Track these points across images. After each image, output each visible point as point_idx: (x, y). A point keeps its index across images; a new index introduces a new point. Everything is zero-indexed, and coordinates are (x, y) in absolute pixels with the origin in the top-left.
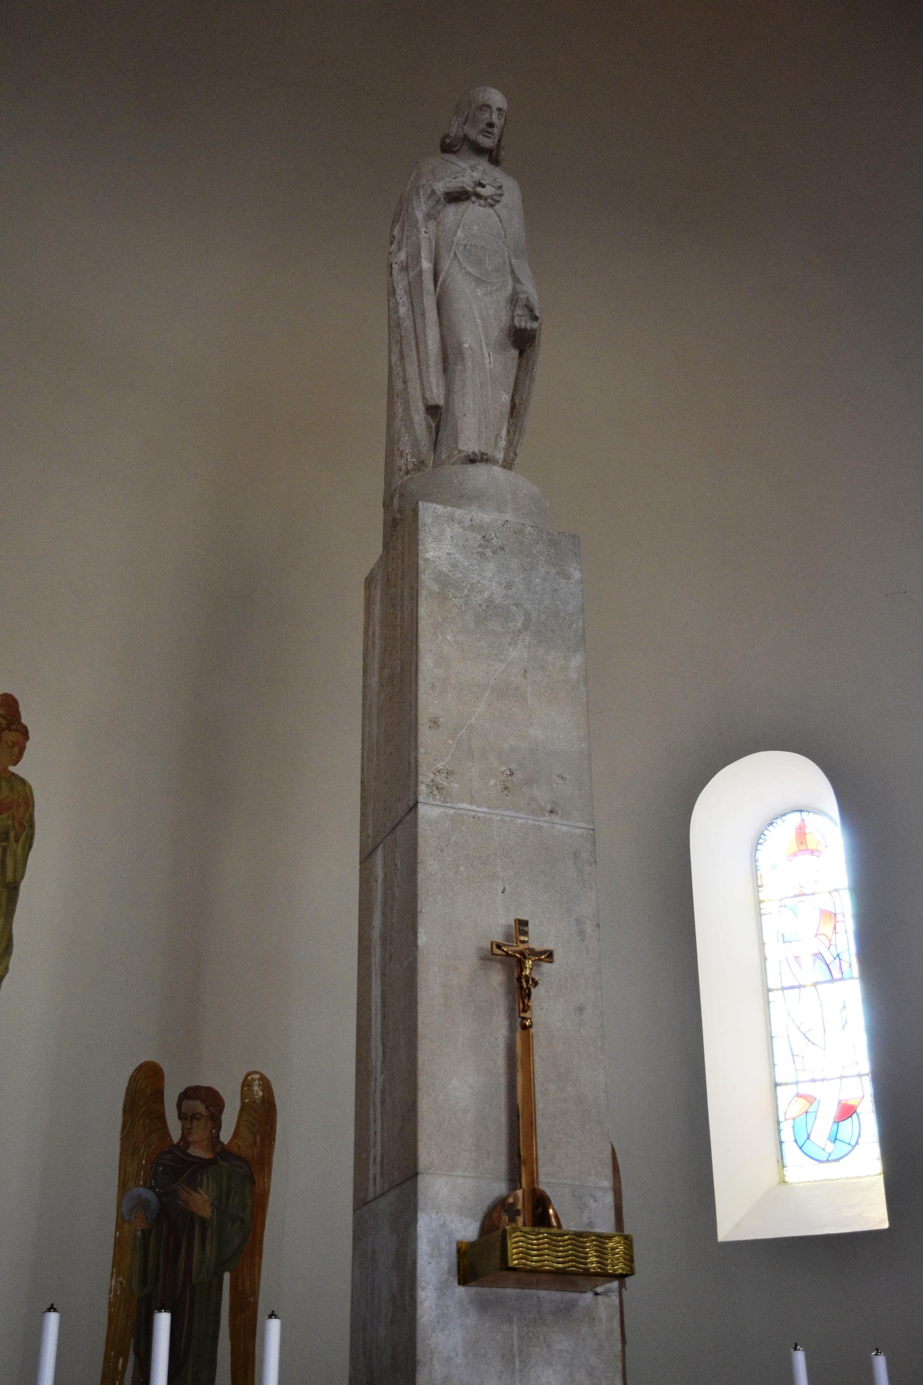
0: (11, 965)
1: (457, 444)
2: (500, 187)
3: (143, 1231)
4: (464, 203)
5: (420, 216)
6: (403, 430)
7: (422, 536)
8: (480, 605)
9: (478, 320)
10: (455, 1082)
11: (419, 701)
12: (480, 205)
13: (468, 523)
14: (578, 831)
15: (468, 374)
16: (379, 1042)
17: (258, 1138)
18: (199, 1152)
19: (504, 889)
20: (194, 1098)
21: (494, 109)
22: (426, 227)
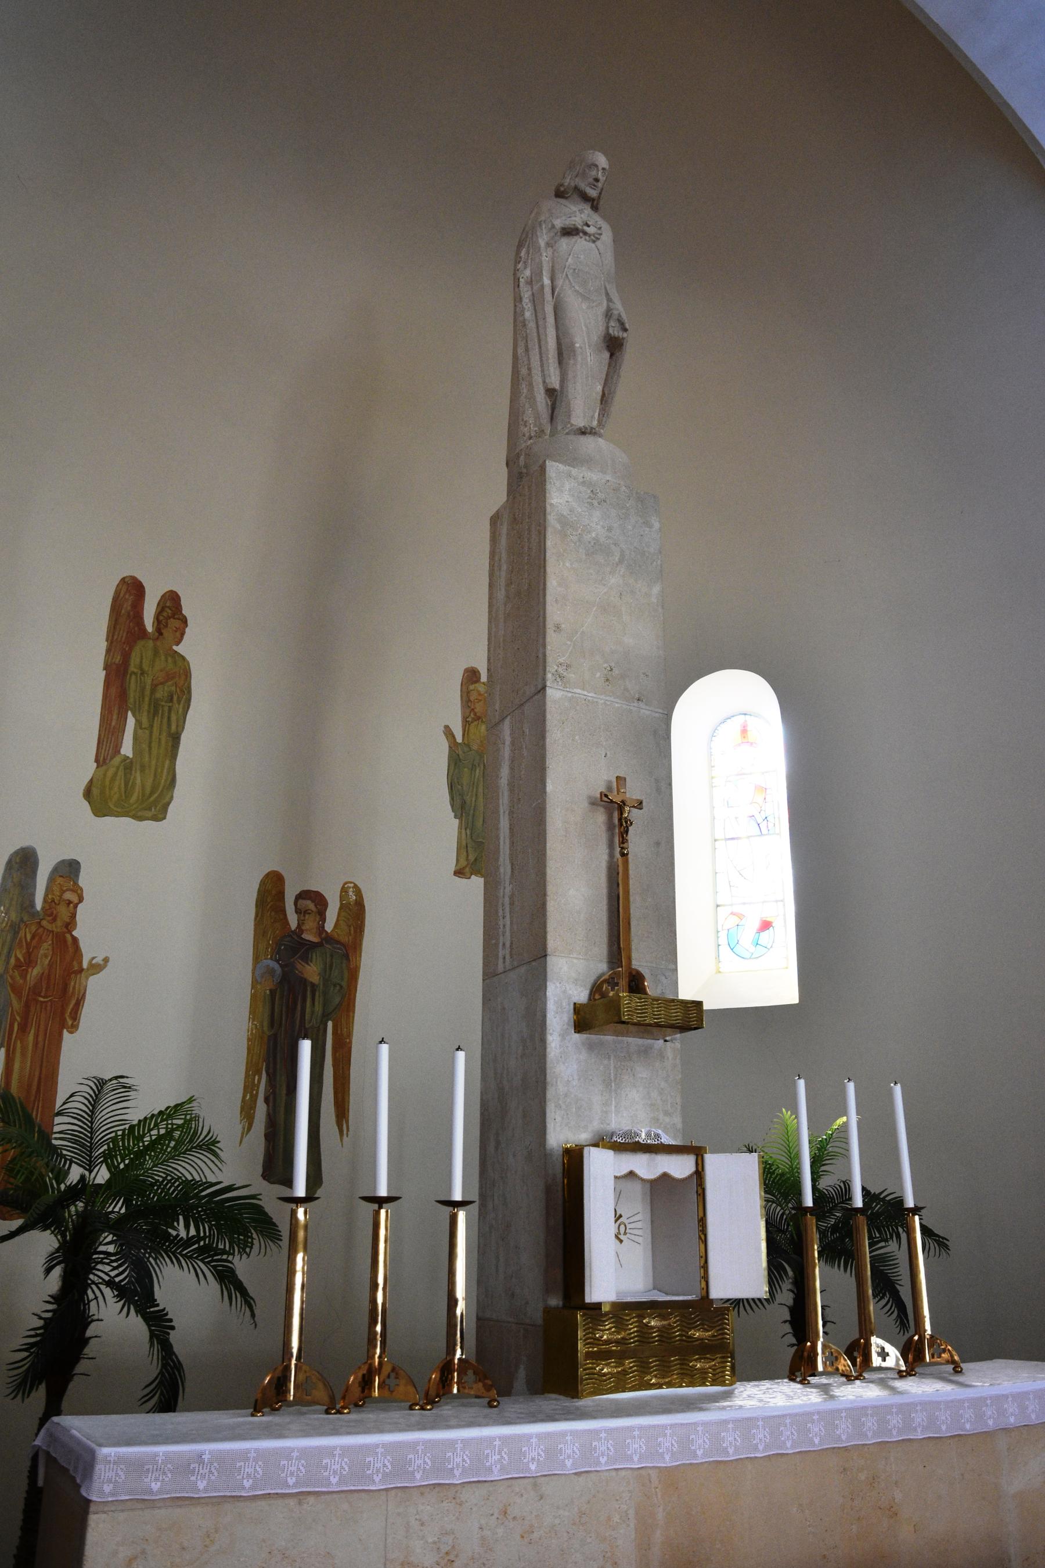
0: (174, 795)
1: (570, 419)
2: (600, 228)
3: (271, 991)
4: (575, 237)
5: (542, 244)
6: (527, 405)
7: (548, 486)
8: (590, 542)
9: (583, 327)
10: (572, 892)
11: (547, 612)
12: (586, 240)
13: (581, 480)
14: (657, 715)
15: (579, 367)
16: (508, 862)
17: (352, 929)
18: (310, 937)
19: (606, 754)
20: (310, 899)
21: (600, 168)
22: (546, 251)
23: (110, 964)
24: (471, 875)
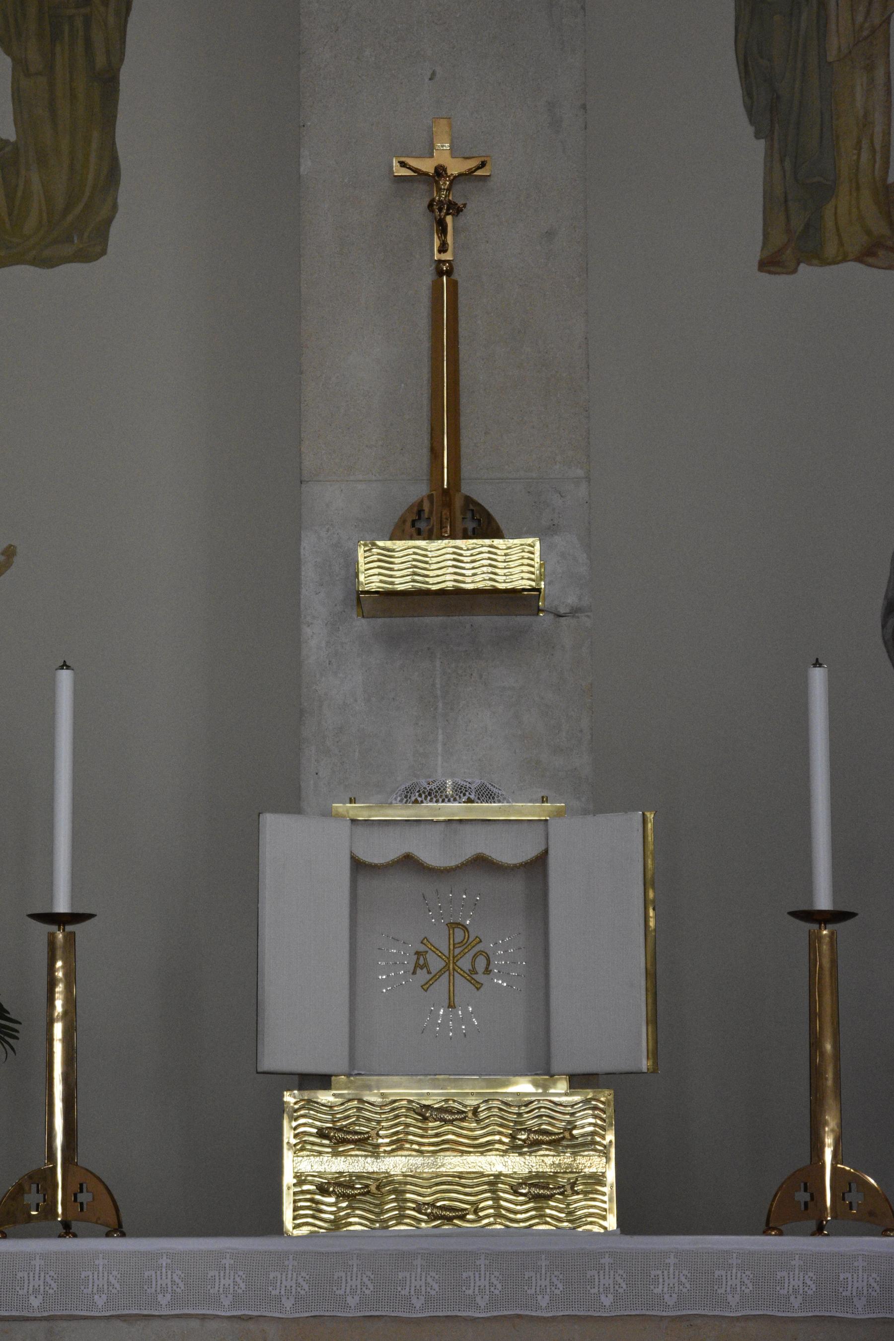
0: (121, 200)
23: (17, 560)
24: (798, 264)
